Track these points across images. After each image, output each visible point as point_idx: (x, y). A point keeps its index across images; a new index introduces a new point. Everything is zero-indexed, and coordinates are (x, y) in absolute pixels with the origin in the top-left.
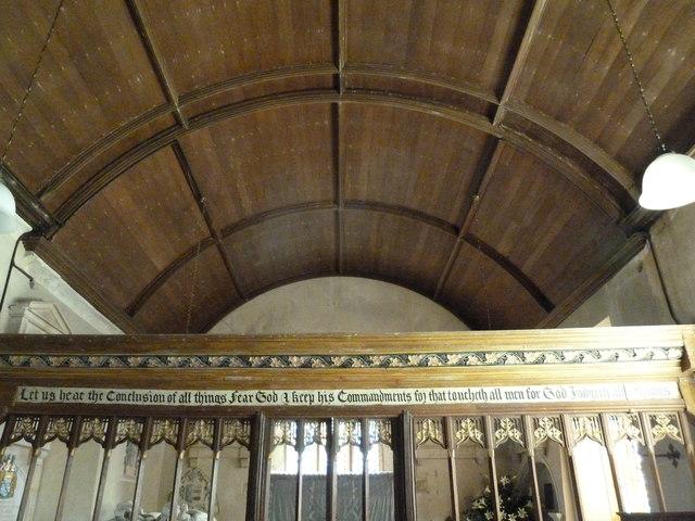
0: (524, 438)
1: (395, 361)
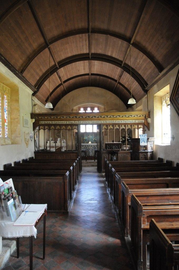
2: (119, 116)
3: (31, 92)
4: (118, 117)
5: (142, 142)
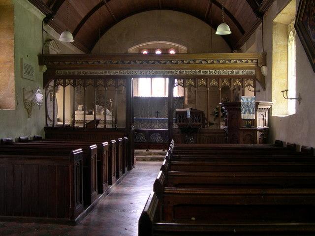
0: (230, 85)
1: (168, 62)
2: (206, 61)
3: (41, 16)
4: (203, 62)
5: (245, 113)
